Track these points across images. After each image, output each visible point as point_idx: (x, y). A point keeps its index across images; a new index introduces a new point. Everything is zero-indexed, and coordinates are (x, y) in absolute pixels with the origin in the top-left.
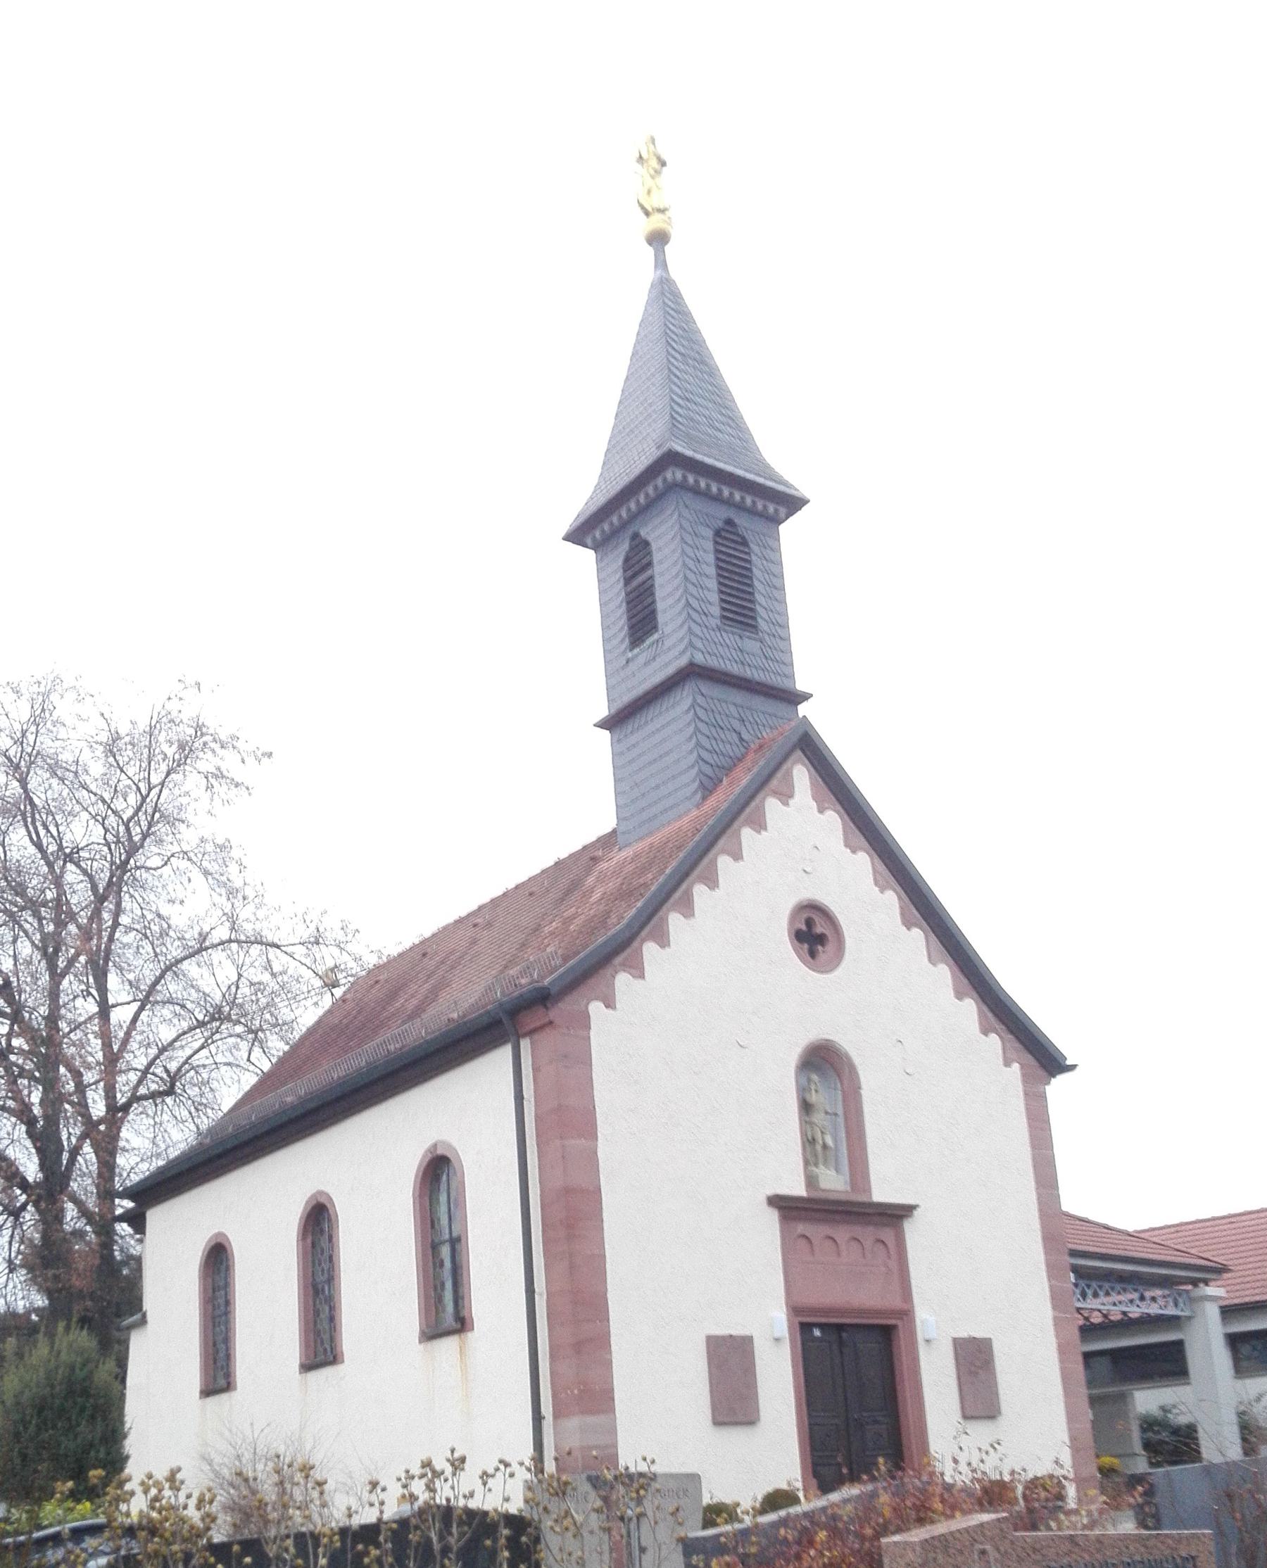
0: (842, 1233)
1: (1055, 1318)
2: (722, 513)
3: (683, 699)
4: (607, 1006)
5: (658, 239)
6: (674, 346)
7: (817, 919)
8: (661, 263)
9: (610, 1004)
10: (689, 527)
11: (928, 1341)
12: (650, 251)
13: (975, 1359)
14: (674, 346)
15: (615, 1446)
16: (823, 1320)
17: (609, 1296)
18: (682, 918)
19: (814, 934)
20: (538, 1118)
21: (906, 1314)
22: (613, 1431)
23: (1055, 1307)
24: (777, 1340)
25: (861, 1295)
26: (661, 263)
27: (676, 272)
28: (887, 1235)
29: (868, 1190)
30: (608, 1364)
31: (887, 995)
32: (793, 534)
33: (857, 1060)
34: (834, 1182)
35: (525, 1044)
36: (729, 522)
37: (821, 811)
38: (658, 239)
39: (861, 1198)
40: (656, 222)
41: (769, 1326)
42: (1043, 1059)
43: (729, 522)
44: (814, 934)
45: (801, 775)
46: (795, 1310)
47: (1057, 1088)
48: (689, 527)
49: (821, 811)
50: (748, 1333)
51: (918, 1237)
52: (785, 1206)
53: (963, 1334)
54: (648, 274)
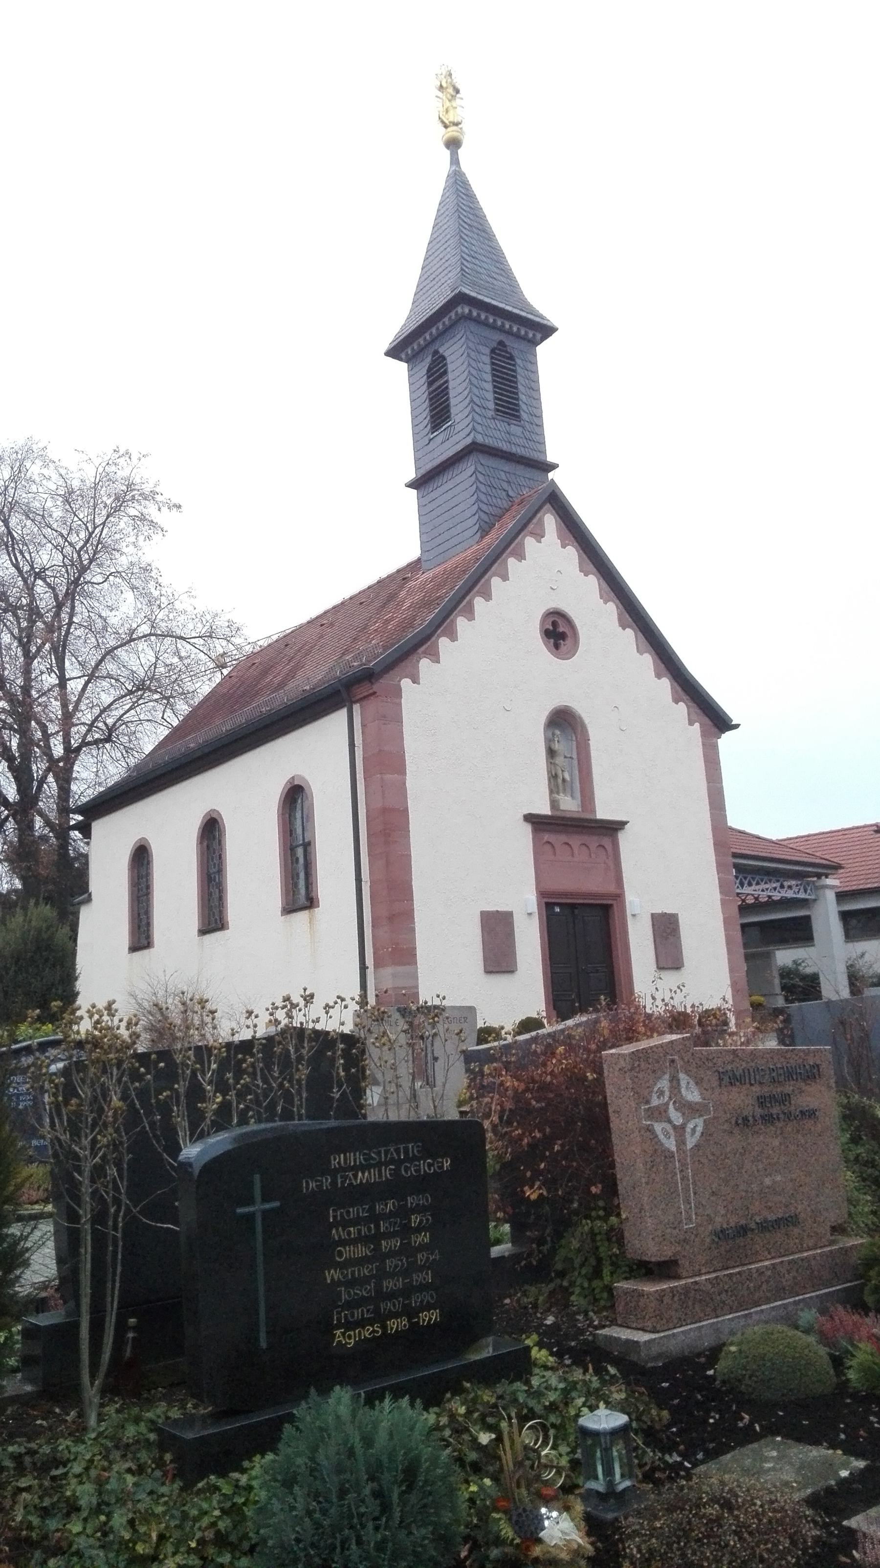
0: (576, 841)
1: (721, 899)
2: (498, 337)
5: (453, 144)
6: (463, 219)
7: (560, 621)
8: (455, 161)
9: (415, 680)
10: (473, 346)
11: (634, 915)
12: (447, 153)
13: (666, 928)
14: (463, 219)
15: (417, 987)
18: (466, 620)
19: (558, 632)
21: (619, 896)
22: (415, 977)
24: (530, 914)
25: (588, 883)
26: (455, 161)
27: (465, 167)
28: (606, 842)
29: (594, 811)
30: (413, 930)
32: (545, 351)
33: (587, 721)
34: (570, 805)
35: (356, 708)
36: (501, 343)
37: (564, 546)
38: (453, 144)
40: (452, 132)
42: (716, 721)
43: (501, 343)
44: (558, 632)
45: (550, 521)
47: (726, 741)
48: (473, 346)
49: (564, 546)
53: (659, 911)
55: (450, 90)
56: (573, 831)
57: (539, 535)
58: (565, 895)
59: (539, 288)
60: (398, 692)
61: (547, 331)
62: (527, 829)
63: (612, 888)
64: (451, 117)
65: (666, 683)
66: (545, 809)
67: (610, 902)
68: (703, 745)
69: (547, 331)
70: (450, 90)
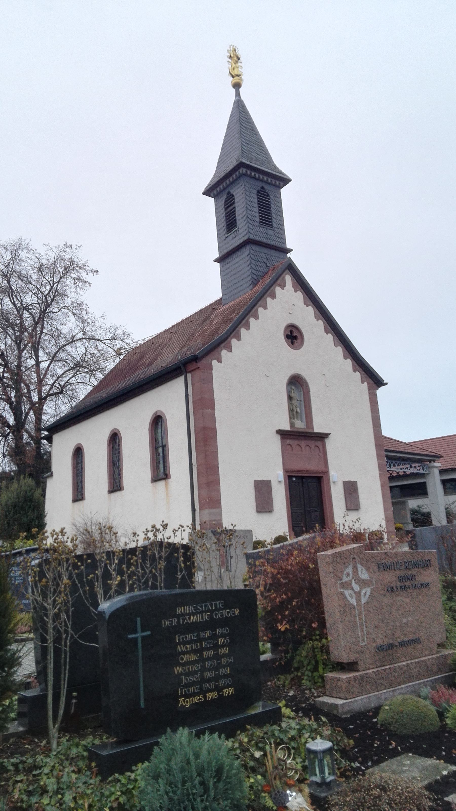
0: (303, 443)
1: (380, 474)
2: (260, 184)
3: (246, 251)
4: (219, 362)
5: (237, 86)
6: (241, 122)
7: (294, 331)
8: (238, 94)
9: (219, 361)
10: (248, 188)
11: (334, 482)
12: (234, 91)
14: (241, 122)
15: (221, 520)
16: (296, 475)
17: (219, 466)
19: (293, 336)
20: (194, 402)
21: (326, 472)
22: (221, 514)
23: (380, 470)
24: (280, 482)
26: (238, 94)
27: (243, 98)
28: (319, 444)
29: (313, 428)
31: (318, 358)
32: (285, 192)
33: (308, 381)
34: (300, 425)
35: (189, 375)
36: (262, 188)
38: (237, 86)
39: (310, 431)
40: (236, 79)
41: (276, 475)
42: (375, 381)
43: (262, 188)
44: (293, 336)
45: (288, 279)
46: (286, 471)
47: (381, 392)
48: (248, 188)
50: (355, 480)
51: (330, 444)
52: (282, 434)
53: (347, 480)
54: (233, 98)
55: (235, 58)
56: (302, 438)
57: (283, 286)
58: (298, 471)
59: (281, 159)
60: (210, 367)
61: (285, 181)
62: (277, 439)
63: (323, 468)
64: (236, 72)
65: (349, 362)
66: (286, 427)
67: (321, 475)
68: (369, 393)
69: (285, 181)
70: (235, 58)
